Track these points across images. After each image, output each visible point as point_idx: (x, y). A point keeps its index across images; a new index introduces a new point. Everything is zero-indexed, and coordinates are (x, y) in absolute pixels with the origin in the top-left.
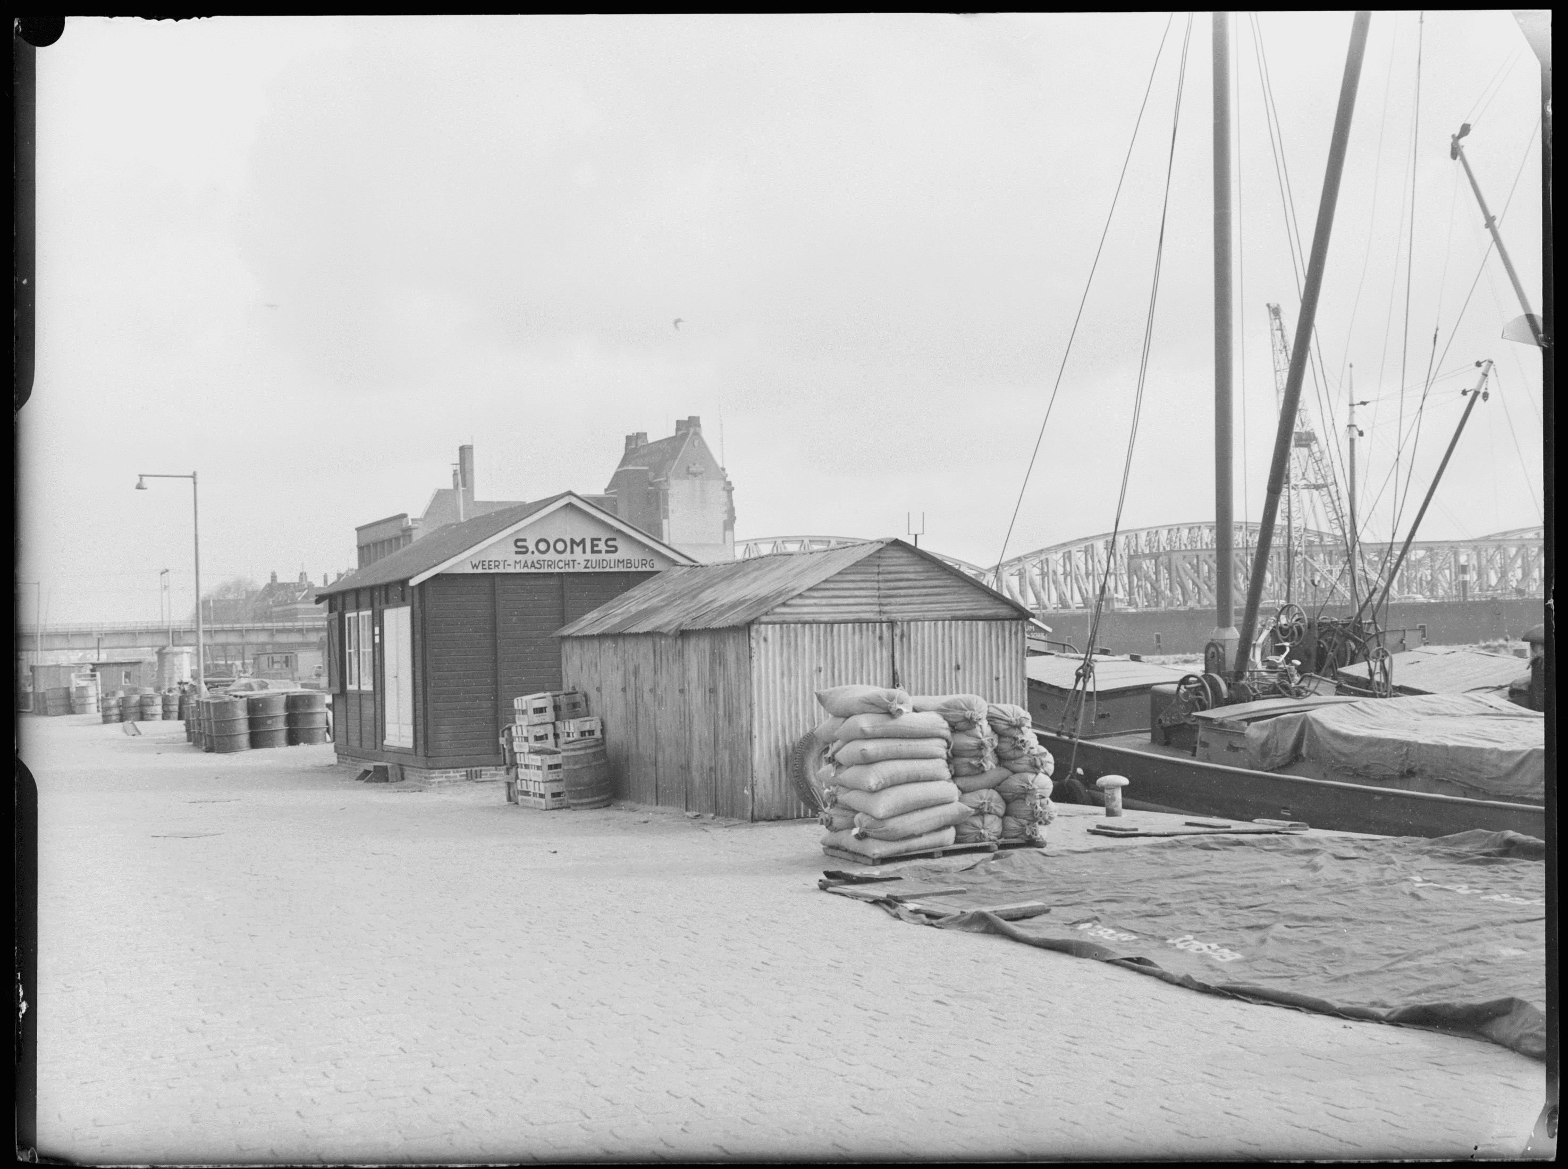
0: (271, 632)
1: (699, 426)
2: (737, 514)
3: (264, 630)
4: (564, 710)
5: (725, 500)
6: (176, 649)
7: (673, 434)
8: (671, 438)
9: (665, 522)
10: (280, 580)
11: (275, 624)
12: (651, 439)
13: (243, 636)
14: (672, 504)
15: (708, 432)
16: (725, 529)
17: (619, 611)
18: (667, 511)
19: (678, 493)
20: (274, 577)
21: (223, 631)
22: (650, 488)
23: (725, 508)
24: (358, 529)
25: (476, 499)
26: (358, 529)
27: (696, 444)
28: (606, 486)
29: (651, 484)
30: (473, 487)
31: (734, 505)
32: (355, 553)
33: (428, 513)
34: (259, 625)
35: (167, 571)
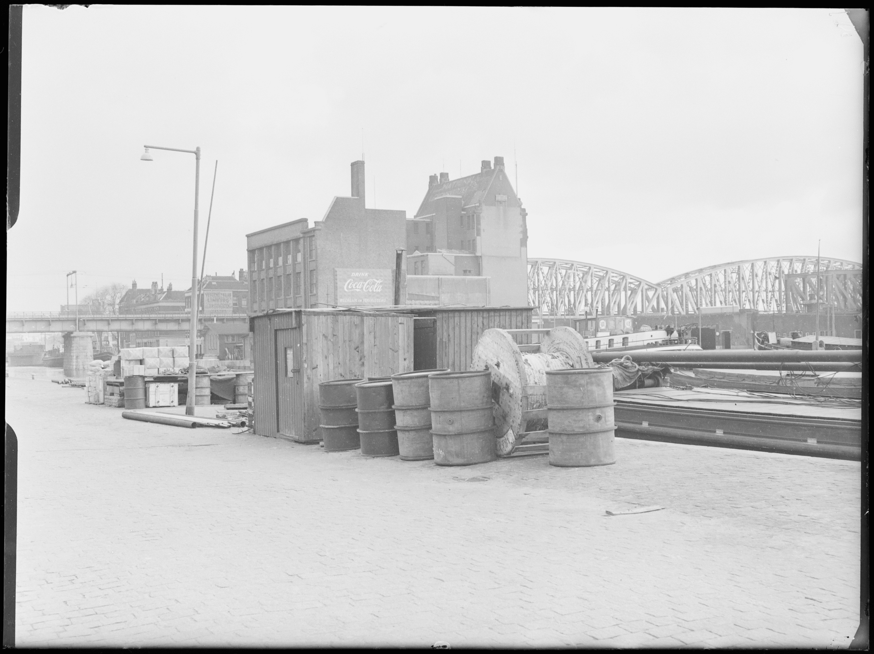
0: (132, 321)
1: (503, 164)
2: (529, 234)
3: (149, 320)
4: (198, 356)
5: (521, 223)
6: (81, 334)
7: (480, 171)
8: (476, 175)
9: (478, 238)
10: (139, 287)
11: (241, 315)
12: (451, 178)
13: (179, 323)
14: (484, 225)
15: (509, 170)
16: (522, 245)
17: (184, 315)
18: (478, 230)
19: (488, 217)
20: (134, 285)
21: (142, 320)
22: (463, 212)
23: (521, 229)
24: (248, 236)
25: (366, 207)
26: (248, 236)
27: (501, 179)
28: (415, 214)
29: (463, 210)
30: (364, 197)
31: (528, 227)
32: (245, 254)
33: (329, 217)
34: (146, 316)
35: (74, 272)
